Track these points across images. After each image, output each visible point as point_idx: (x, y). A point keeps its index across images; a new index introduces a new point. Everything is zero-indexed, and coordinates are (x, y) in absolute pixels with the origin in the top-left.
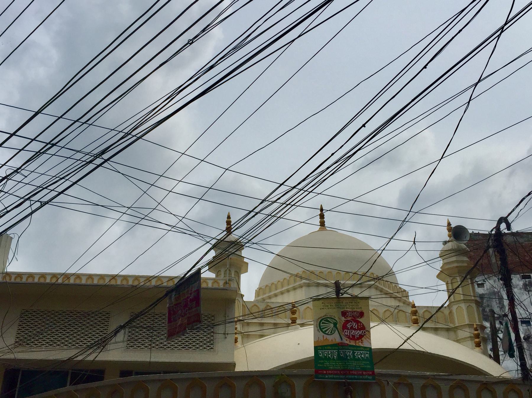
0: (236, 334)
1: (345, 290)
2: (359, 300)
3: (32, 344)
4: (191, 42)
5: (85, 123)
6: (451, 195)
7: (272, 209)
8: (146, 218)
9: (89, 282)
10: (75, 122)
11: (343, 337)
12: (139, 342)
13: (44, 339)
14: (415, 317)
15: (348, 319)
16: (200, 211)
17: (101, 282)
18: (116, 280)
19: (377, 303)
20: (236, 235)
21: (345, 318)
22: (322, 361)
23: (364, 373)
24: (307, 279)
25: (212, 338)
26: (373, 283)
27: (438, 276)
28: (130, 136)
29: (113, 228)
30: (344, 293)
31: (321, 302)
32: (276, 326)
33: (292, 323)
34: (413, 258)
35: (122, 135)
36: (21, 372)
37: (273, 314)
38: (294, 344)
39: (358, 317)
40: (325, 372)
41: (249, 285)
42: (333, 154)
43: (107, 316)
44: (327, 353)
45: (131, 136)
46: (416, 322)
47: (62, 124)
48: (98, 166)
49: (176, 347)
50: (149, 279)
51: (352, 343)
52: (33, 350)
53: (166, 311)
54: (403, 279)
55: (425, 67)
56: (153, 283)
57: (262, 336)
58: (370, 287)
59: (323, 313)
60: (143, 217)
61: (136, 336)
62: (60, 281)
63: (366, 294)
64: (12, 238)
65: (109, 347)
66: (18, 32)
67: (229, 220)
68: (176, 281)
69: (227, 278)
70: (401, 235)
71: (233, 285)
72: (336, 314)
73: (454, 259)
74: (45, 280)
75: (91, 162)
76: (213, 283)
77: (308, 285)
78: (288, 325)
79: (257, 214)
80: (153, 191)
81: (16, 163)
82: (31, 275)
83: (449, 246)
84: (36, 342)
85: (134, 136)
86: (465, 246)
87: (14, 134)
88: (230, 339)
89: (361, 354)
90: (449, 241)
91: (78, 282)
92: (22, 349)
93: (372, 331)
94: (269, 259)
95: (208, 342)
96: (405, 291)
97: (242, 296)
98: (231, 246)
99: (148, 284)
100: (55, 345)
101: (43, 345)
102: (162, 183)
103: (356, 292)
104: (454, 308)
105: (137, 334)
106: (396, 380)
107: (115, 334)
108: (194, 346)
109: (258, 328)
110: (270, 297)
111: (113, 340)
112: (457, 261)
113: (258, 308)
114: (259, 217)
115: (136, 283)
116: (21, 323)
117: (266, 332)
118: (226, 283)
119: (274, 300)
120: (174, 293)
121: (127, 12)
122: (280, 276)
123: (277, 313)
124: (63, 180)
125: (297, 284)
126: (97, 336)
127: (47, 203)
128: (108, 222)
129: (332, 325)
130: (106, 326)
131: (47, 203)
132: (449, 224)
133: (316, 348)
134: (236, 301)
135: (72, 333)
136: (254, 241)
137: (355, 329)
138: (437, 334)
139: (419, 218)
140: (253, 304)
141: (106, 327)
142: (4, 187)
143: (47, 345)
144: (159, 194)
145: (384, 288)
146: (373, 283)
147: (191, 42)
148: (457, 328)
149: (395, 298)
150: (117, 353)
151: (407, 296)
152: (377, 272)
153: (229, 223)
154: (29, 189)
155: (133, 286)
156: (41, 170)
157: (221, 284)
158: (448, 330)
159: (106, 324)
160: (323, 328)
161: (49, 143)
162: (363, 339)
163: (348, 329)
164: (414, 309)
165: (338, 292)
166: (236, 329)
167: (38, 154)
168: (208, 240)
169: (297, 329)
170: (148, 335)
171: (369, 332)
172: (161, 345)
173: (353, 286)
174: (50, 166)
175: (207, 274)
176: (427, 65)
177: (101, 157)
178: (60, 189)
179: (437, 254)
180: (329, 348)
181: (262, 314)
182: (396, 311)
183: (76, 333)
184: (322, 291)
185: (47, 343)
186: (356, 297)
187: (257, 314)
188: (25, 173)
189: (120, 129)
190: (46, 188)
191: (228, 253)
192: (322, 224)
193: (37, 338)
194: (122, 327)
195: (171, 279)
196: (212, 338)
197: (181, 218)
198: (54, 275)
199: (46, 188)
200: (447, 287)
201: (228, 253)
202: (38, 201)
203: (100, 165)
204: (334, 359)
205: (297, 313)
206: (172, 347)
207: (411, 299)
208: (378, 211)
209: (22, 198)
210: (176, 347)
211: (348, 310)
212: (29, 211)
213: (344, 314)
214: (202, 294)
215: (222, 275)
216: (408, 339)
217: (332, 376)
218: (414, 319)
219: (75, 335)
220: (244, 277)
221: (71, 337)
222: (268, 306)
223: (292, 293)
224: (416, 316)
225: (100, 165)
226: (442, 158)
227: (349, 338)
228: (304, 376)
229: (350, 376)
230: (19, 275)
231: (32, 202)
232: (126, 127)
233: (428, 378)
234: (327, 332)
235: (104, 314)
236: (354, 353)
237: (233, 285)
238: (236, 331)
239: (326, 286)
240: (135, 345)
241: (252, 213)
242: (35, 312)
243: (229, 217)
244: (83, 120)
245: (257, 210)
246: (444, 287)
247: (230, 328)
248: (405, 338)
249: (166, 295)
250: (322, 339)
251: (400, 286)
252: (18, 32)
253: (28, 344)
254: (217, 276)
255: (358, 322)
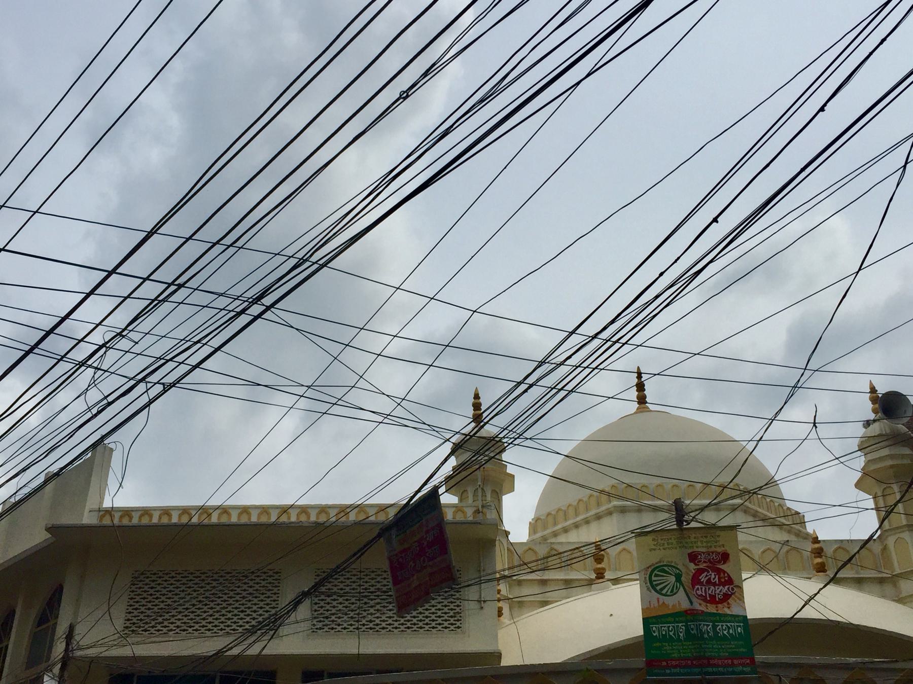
0: (499, 600)
1: (693, 514)
2: (718, 533)
3: (152, 630)
4: (405, 96)
5: (231, 245)
6: (881, 335)
7: (550, 380)
8: (340, 402)
9: (244, 520)
10: (214, 244)
11: (694, 600)
12: (333, 621)
13: (173, 620)
14: (819, 560)
15: (701, 567)
16: (434, 384)
17: (264, 519)
18: (289, 514)
19: (752, 538)
20: (490, 430)
21: (696, 565)
22: (658, 644)
23: (736, 662)
24: (622, 498)
25: (458, 609)
26: (738, 501)
27: (858, 485)
28: (308, 264)
29: (280, 422)
30: (692, 520)
31: (649, 538)
32: (568, 584)
33: (598, 578)
34: (815, 453)
35: (293, 262)
36: (135, 679)
37: (563, 564)
38: (609, 614)
39: (719, 562)
40: (664, 663)
41: (518, 514)
42: (661, 274)
43: (276, 577)
44: (664, 628)
45: (308, 265)
46: (821, 568)
47: (193, 250)
48: (256, 318)
49: (396, 628)
50: (344, 510)
51: (711, 609)
52: (153, 639)
53: (386, 565)
54: (795, 493)
55: (822, 109)
56: (352, 517)
57: (545, 603)
58: (734, 509)
59: (654, 558)
60: (334, 401)
61: (328, 610)
62: (195, 520)
63: (727, 521)
64: (112, 450)
65: (283, 630)
66: (119, 93)
67: (477, 401)
68: (392, 513)
69: (479, 503)
70: (790, 413)
71: (491, 515)
72: (676, 557)
73: (885, 452)
74: (170, 519)
75: (243, 311)
76: (455, 513)
77: (623, 510)
78: (590, 583)
79: (531, 386)
80: (349, 356)
81: (120, 319)
82: (146, 512)
83: (875, 429)
84: (159, 627)
85: (314, 263)
86: (904, 429)
87: (114, 271)
88: (490, 609)
89: (729, 628)
90: (874, 421)
91: (224, 520)
92: (139, 639)
93: (746, 586)
94: (552, 464)
95: (451, 617)
96: (797, 513)
97: (507, 533)
98: (490, 445)
99: (344, 519)
100: (190, 630)
101: (171, 630)
102: (364, 340)
103: (710, 517)
104: (891, 541)
105: (328, 607)
106: (794, 674)
107: (295, 608)
108: (427, 624)
109: (536, 589)
110: (555, 534)
111: (293, 618)
112: (891, 457)
113: (535, 553)
114: (536, 392)
115: (323, 519)
116: (132, 595)
117: (549, 596)
118: (477, 512)
119: (562, 539)
120: (394, 532)
121: (296, 46)
122: (573, 495)
123: (569, 562)
124: (199, 345)
125: (603, 508)
126: (261, 612)
127: (173, 385)
128: (273, 414)
129: (673, 579)
130: (275, 594)
131: (173, 385)
132: (873, 390)
133: (647, 622)
134: (497, 543)
135: (218, 608)
136: (528, 434)
137: (714, 584)
138: (860, 589)
139: (819, 380)
140: (526, 548)
141: (275, 597)
142: (101, 362)
143: (178, 630)
144: (358, 361)
145: (760, 510)
146: (738, 501)
147: (405, 96)
148: (900, 576)
149: (781, 526)
150: (296, 641)
151: (803, 523)
152: (746, 481)
153: (477, 406)
154: (142, 363)
155: (317, 524)
156: (161, 330)
157: (470, 512)
158: (881, 581)
159: (275, 590)
160: (658, 585)
161: (172, 283)
162: (730, 601)
163: (701, 584)
164: (817, 546)
165: (680, 521)
166: (499, 592)
167: (155, 303)
168: (448, 436)
169: (606, 589)
170: (346, 607)
171: (740, 588)
172: (371, 625)
173: (703, 509)
174: (175, 323)
175: (447, 499)
176: (825, 105)
177: (259, 304)
178: (194, 361)
179: (854, 444)
180: (670, 619)
181: (544, 564)
182: (786, 548)
183: (224, 608)
184: (648, 520)
185: (178, 627)
186: (713, 527)
187: (535, 564)
188: (135, 336)
189: (289, 252)
190: (171, 360)
191: (479, 458)
192: (642, 400)
193: (160, 619)
194: (305, 595)
195: (383, 508)
196: (458, 609)
197: (399, 401)
198: (185, 511)
199: (171, 360)
200: (876, 503)
201: (479, 458)
202: (158, 383)
203: (259, 316)
204: (679, 640)
205: (605, 559)
206: (390, 627)
207: (810, 528)
208: (746, 372)
209: (132, 379)
210: (396, 628)
211: (700, 550)
212: (144, 400)
213: (693, 557)
214: (448, 530)
215: (470, 500)
216: (811, 598)
217: (678, 670)
218: (817, 564)
219: (224, 612)
220: (507, 500)
221: (217, 615)
222: (552, 549)
223: (594, 525)
224: (821, 557)
225: (259, 316)
226: (860, 269)
227: (705, 600)
228: (628, 671)
229: (710, 669)
230: (127, 512)
231: (149, 385)
232: (298, 248)
233: (853, 669)
234: (664, 592)
235: (271, 573)
236: (714, 627)
237: (491, 515)
238: (498, 596)
239: (656, 509)
240: (327, 625)
241: (524, 384)
242: (155, 574)
243: (477, 396)
244: (228, 240)
245: (530, 380)
246: (871, 504)
247: (488, 591)
248: (806, 598)
249: (379, 536)
250: (656, 605)
251: (789, 504)
252: (119, 93)
253: (146, 631)
254: (461, 500)
255: (719, 571)
